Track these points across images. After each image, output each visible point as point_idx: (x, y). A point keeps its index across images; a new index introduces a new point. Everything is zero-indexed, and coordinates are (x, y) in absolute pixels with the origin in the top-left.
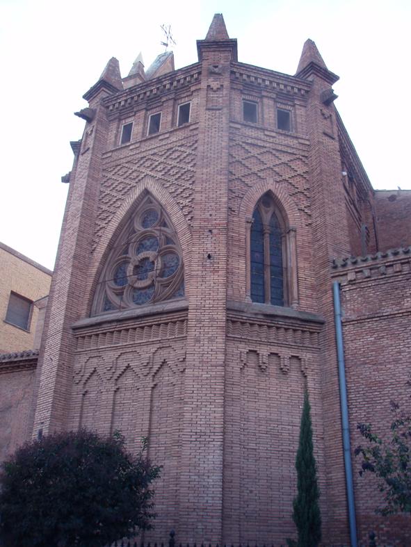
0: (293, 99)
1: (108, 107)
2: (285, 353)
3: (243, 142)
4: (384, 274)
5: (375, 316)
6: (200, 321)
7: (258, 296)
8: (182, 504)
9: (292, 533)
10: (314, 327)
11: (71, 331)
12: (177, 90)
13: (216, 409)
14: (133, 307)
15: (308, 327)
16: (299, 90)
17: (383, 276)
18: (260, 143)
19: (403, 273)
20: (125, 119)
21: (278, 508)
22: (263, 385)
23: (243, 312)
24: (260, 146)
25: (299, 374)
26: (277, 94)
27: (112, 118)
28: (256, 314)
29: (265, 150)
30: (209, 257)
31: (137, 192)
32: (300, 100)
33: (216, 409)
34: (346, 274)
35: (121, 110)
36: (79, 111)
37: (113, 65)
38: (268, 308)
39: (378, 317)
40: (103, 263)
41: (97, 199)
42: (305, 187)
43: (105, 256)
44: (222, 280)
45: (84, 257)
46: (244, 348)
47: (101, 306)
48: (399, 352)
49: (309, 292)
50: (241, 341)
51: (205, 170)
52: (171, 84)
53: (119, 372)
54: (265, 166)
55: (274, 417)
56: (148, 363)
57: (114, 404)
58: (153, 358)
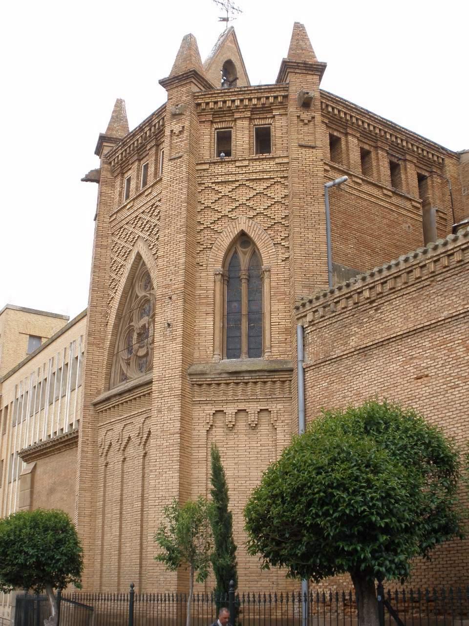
0: (272, 109)
1: (110, 163)
2: (253, 408)
3: (212, 183)
4: (333, 312)
5: (328, 360)
6: (161, 392)
7: (231, 351)
8: (149, 561)
9: (257, 581)
10: (285, 376)
11: (92, 408)
12: (156, 135)
13: (173, 475)
14: (136, 376)
15: (277, 376)
16: (276, 97)
17: (334, 314)
18: (231, 178)
19: (359, 304)
20: (126, 172)
21: (244, 559)
22: (231, 443)
23: (206, 374)
24: (232, 182)
25: (270, 427)
26: (251, 111)
27: (116, 174)
28: (220, 374)
29: (237, 184)
30: (169, 325)
31: (133, 256)
32: (279, 109)
33: (173, 475)
34: (305, 316)
35: (121, 164)
36: (84, 176)
37: (189, 45)
38: (244, 363)
39: (329, 360)
40: (115, 334)
41: (108, 267)
42: (283, 215)
43: (116, 326)
44: (179, 347)
45: (100, 331)
46: (210, 409)
47: (118, 378)
48: (344, 397)
49: (282, 337)
50: (206, 403)
51: (167, 231)
52: (150, 130)
53: (124, 443)
54: (237, 204)
55: (242, 473)
56: (139, 433)
57: (123, 472)
58: (143, 428)
